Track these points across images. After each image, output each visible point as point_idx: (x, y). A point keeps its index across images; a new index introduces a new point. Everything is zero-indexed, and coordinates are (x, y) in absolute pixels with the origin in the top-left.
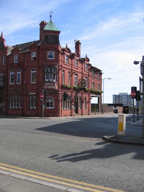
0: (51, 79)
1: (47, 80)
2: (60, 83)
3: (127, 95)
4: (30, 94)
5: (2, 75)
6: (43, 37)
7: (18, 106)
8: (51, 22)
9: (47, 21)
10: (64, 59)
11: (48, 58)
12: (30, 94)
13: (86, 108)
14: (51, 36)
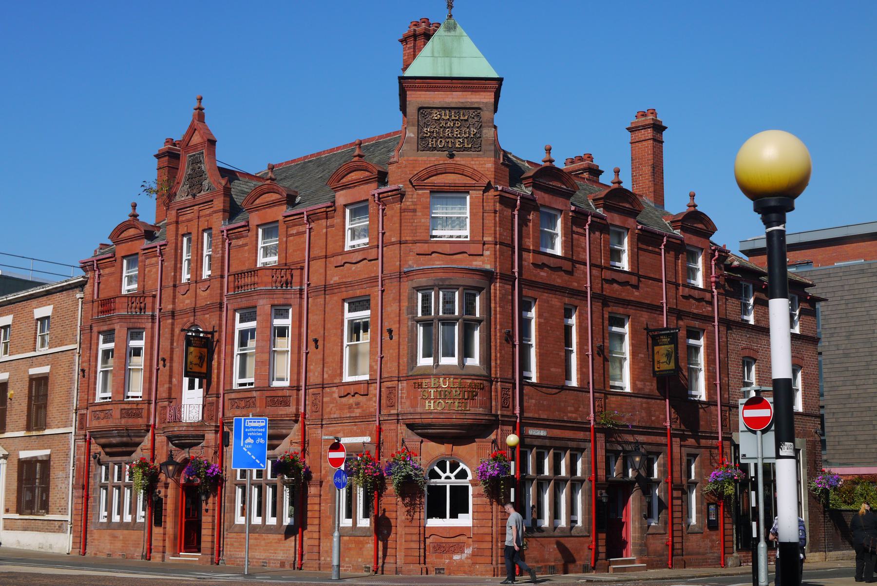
0: (449, 353)
1: (429, 361)
13: (246, 245)
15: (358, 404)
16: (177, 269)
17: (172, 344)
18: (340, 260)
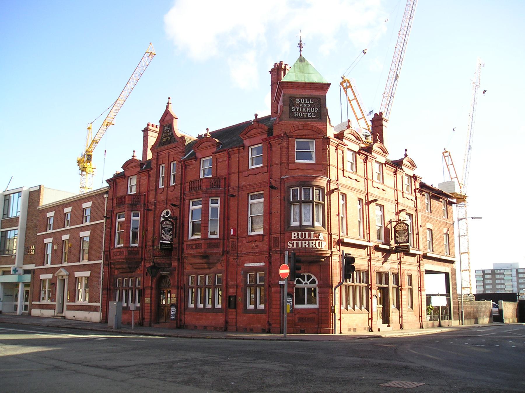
2: (335, 230)
3: (517, 270)
4: (246, 265)
5: (167, 213)
6: (281, 103)
7: (203, 301)
8: (301, 59)
9: (289, 59)
10: (341, 158)
11: (297, 161)
12: (246, 265)
14: (305, 98)
15: (257, 246)
16: (157, 182)
17: (154, 218)
18: (246, 174)
